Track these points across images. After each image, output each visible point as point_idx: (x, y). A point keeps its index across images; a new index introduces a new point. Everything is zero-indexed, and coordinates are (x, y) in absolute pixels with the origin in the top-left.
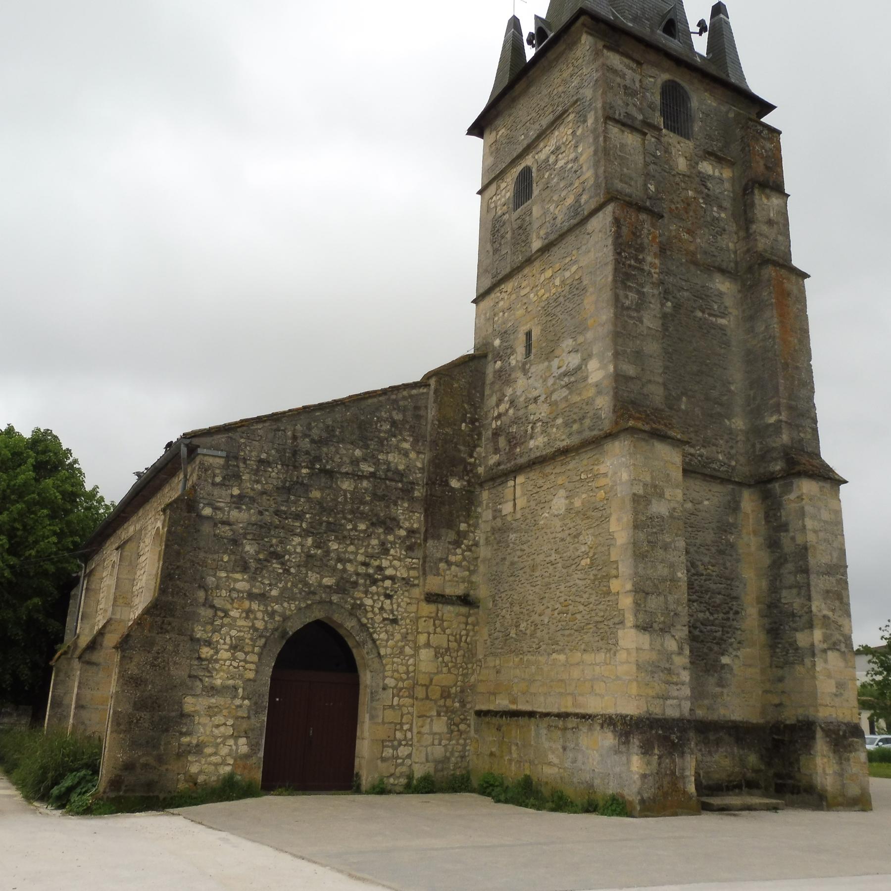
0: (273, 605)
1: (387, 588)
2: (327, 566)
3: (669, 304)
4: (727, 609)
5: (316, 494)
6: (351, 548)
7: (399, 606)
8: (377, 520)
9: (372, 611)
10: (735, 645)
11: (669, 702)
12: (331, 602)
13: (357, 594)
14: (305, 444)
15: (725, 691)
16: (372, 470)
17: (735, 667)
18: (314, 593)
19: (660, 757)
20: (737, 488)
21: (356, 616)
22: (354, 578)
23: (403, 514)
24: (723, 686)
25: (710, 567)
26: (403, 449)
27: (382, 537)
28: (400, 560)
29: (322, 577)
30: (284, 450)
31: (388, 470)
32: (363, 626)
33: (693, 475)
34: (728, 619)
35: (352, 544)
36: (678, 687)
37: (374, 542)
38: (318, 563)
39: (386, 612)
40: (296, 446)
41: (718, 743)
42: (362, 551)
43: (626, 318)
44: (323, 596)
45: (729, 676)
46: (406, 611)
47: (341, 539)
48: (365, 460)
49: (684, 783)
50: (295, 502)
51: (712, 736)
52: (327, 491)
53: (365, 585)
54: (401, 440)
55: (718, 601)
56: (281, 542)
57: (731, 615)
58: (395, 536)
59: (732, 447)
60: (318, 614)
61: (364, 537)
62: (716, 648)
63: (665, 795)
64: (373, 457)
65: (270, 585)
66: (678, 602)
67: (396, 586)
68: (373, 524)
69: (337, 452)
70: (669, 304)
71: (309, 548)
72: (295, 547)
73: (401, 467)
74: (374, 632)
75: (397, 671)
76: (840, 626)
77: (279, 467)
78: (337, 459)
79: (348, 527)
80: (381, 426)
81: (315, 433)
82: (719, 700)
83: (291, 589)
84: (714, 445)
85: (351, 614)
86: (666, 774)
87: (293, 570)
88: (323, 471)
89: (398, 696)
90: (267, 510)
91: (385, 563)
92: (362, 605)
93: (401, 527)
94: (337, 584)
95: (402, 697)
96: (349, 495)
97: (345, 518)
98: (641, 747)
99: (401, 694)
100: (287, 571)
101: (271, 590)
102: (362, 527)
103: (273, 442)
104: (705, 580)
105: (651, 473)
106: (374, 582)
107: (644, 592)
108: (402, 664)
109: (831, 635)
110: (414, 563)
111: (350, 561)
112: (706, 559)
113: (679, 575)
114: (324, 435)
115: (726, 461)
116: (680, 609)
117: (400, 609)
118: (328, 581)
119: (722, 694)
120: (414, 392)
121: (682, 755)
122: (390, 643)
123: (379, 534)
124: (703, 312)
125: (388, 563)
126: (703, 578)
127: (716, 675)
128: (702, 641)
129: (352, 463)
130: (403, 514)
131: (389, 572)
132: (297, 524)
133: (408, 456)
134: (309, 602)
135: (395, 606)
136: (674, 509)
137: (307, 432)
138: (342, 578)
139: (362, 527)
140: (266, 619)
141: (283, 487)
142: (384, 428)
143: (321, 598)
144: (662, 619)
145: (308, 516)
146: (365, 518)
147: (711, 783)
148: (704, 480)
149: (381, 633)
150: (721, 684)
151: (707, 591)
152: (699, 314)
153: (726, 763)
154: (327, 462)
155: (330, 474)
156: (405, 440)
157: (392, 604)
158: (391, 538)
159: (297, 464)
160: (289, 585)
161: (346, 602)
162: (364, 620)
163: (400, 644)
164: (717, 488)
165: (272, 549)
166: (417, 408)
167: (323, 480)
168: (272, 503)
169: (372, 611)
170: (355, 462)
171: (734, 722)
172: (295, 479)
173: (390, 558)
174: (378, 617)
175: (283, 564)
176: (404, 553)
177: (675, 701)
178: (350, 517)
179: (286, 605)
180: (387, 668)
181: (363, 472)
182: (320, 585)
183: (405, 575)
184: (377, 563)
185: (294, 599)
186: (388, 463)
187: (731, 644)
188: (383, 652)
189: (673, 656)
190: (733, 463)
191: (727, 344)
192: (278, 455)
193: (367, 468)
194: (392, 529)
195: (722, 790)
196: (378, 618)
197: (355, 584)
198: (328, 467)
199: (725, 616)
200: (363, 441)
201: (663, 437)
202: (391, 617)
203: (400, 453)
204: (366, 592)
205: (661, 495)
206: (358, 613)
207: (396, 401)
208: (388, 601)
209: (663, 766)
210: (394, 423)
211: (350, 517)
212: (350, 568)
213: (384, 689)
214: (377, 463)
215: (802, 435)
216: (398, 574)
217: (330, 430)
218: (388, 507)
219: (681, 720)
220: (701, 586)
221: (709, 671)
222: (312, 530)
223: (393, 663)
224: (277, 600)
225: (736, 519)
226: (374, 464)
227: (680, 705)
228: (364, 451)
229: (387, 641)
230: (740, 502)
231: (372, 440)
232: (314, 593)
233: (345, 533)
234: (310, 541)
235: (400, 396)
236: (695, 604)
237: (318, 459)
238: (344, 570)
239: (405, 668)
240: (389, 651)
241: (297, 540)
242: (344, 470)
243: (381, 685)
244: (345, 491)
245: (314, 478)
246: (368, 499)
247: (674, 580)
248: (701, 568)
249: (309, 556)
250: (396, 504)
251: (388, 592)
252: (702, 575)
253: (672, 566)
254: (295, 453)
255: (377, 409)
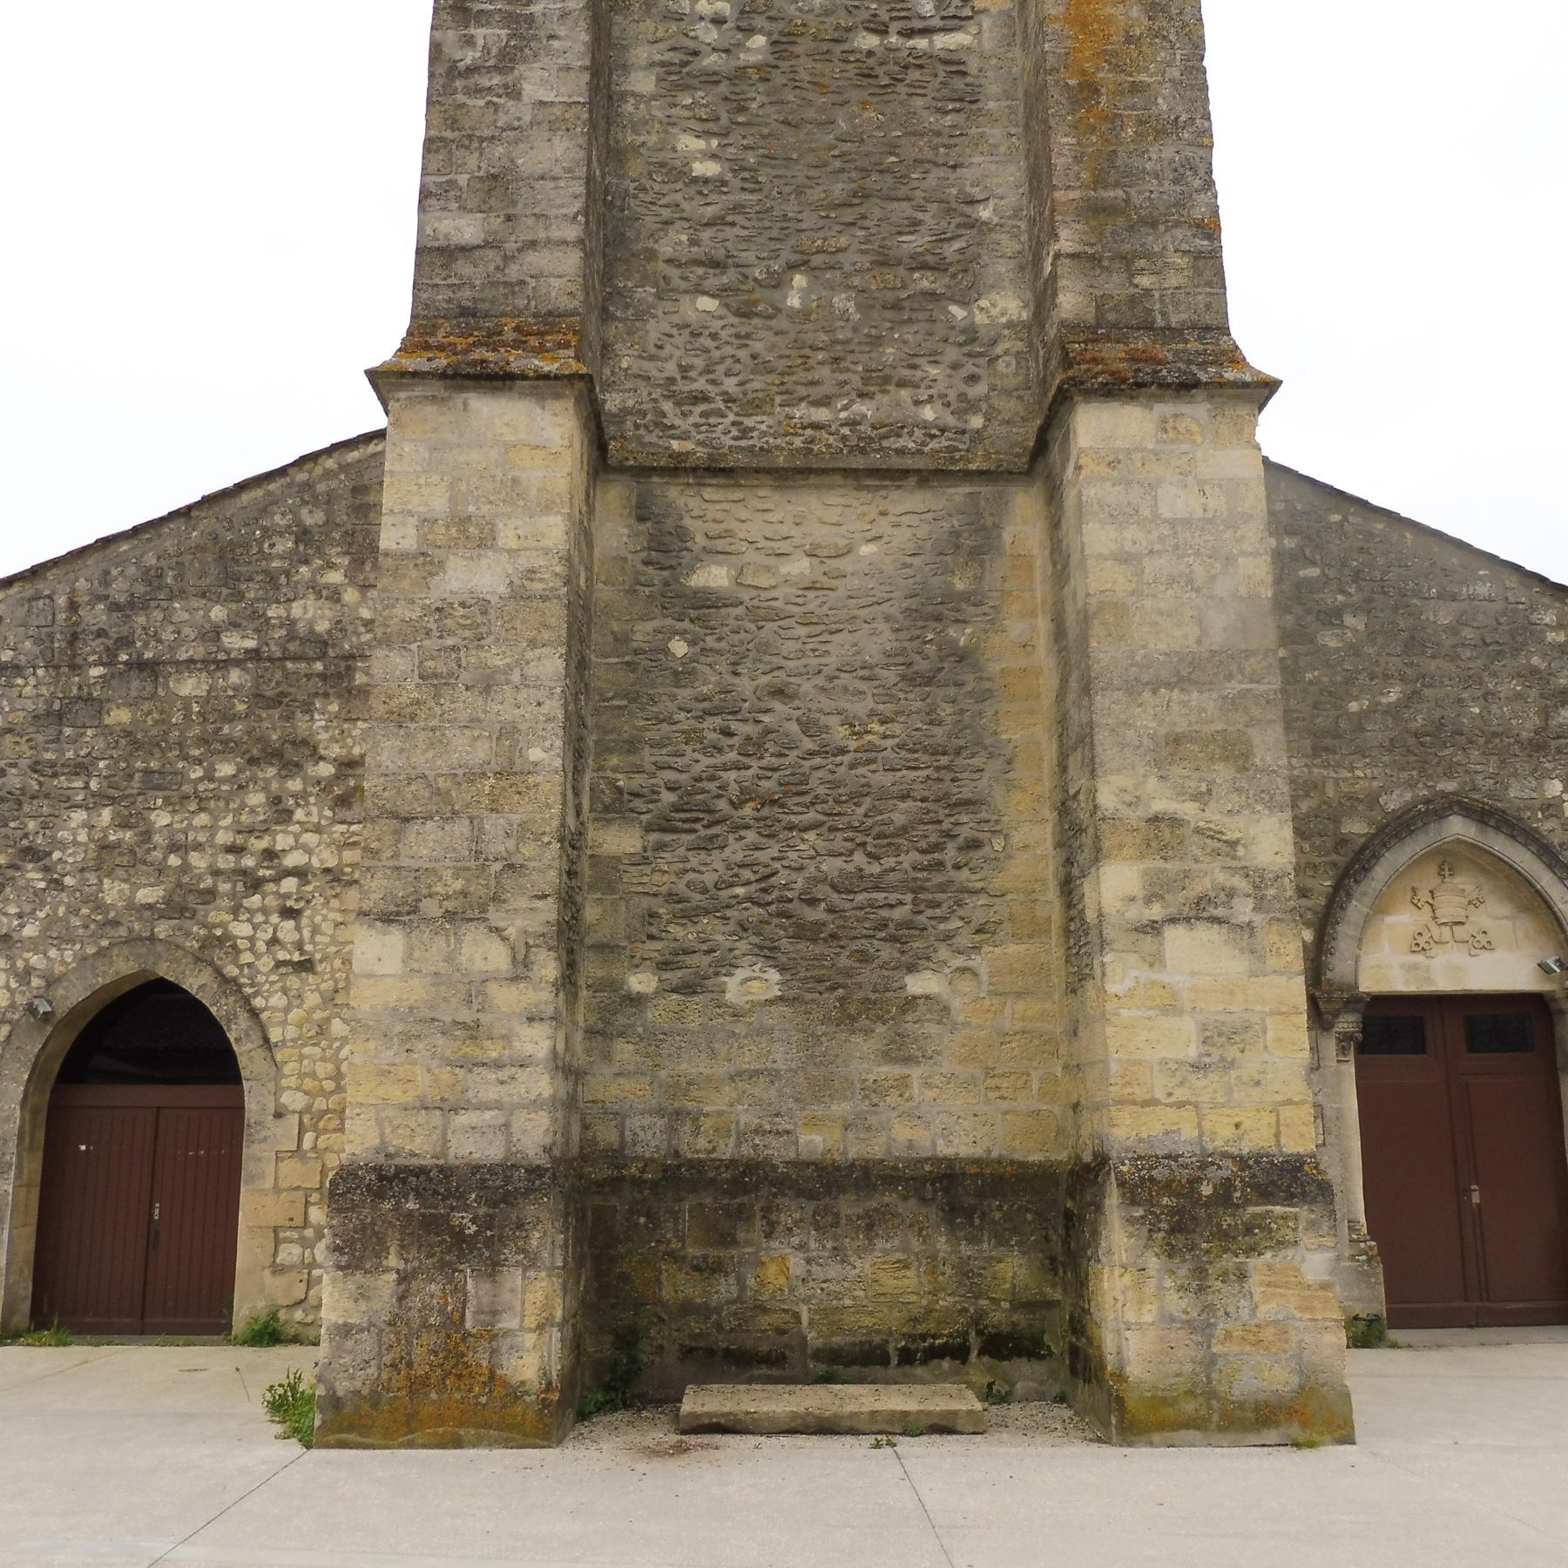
0: (27, 955)
1: (287, 896)
2: (145, 862)
3: (759, 41)
4: (933, 839)
5: (120, 716)
6: (202, 819)
7: (315, 930)
8: (263, 750)
9: (252, 949)
10: (964, 940)
11: (463, 1119)
12: (152, 938)
13: (214, 917)
14: (97, 616)
15: (916, 1073)
16: (251, 644)
17: (956, 1003)
18: (115, 923)
19: (404, 1278)
20: (985, 490)
21: (212, 964)
22: (208, 882)
23: (326, 728)
24: (908, 1060)
25: (876, 727)
26: (327, 586)
27: (274, 786)
28: (318, 829)
29: (135, 888)
30: (51, 636)
31: (292, 636)
32: (224, 980)
33: (813, 480)
34: (939, 865)
35: (201, 809)
36: (503, 1074)
37: (256, 799)
38: (125, 860)
39: (283, 947)
40: (77, 624)
41: (871, 1225)
42: (227, 821)
43: (461, 98)
44: (137, 926)
45: (932, 1029)
46: (334, 941)
47: (176, 803)
48: (234, 625)
49: (494, 1352)
50: (73, 741)
51: (848, 1206)
52: (146, 706)
53: (233, 895)
54: (322, 568)
55: (899, 819)
56: (44, 826)
57: (950, 854)
58: (305, 780)
59: (973, 379)
60: (124, 966)
61: (230, 792)
62: (887, 952)
63: (416, 1386)
64: (254, 615)
65: (20, 916)
66: (523, 831)
67: (309, 888)
68: (252, 761)
69: (167, 619)
70: (759, 41)
71: (105, 830)
72: (74, 832)
73: (322, 627)
74: (256, 994)
75: (313, 1075)
76: (1233, 844)
77: (40, 672)
78: (168, 635)
79: (193, 776)
80: (272, 546)
81: (119, 590)
82: (892, 1099)
83: (65, 919)
84: (902, 384)
85: (198, 960)
86: (425, 1326)
87: (68, 881)
88: (141, 666)
89: (315, 1128)
90: (14, 765)
91: (282, 841)
92: (227, 936)
93: (322, 758)
94: (168, 901)
95: (326, 1130)
96: (196, 708)
97: (186, 758)
98: (337, 1249)
99: (321, 1124)
100: (57, 884)
101: (22, 926)
102: (226, 769)
103: (25, 625)
104: (852, 766)
105: (452, 486)
106: (256, 885)
107: (394, 815)
108: (323, 1059)
109: (1186, 874)
110: (354, 834)
111: (198, 847)
112: (861, 708)
113: (535, 754)
114: (140, 589)
115: (951, 421)
116: (528, 849)
117: (318, 938)
118: (146, 895)
119: (904, 1082)
120: (353, 456)
121: (493, 1268)
122: (295, 1014)
123: (267, 781)
124: (883, 32)
125: (291, 840)
126: (847, 759)
127: (880, 1029)
128: (833, 936)
129: (202, 636)
130: (326, 728)
131: (293, 860)
132: (79, 784)
133: (338, 601)
134: (105, 943)
135: (306, 933)
136: (530, 574)
137: (101, 591)
138: (179, 885)
139: (226, 769)
140: (13, 985)
141: (48, 714)
142: (279, 548)
143: (131, 930)
144: (458, 885)
145: (102, 764)
146: (232, 751)
147: (837, 1340)
148: (859, 488)
149: (271, 994)
150: (900, 1052)
151: (856, 797)
152: (870, 41)
153: (909, 1284)
154: (146, 644)
155: (150, 669)
156: (331, 566)
157: (298, 928)
158: (295, 785)
159: (78, 660)
160: (61, 911)
161: (187, 934)
162: (231, 970)
163: (318, 1015)
164: (909, 501)
165: (25, 842)
166: (356, 491)
167: (135, 684)
168: (25, 747)
169: (252, 949)
170: (213, 634)
171: (950, 1162)
172: (75, 691)
173: (295, 828)
174: (264, 959)
175: (46, 869)
176: (328, 813)
177: (488, 1115)
178: (197, 752)
179: (53, 953)
180: (286, 1070)
181: (228, 652)
182: (131, 906)
183: (332, 863)
184: (264, 843)
185: (72, 941)
186: (290, 623)
187: (947, 937)
188: (275, 1035)
189: (492, 988)
190: (977, 422)
191: (968, 100)
192: (37, 650)
193: (236, 642)
194: (297, 765)
195: (884, 1361)
196: (265, 963)
197: (211, 893)
198: (148, 655)
199: (925, 860)
200: (229, 583)
201: (497, 380)
202: (296, 957)
203: (319, 596)
204: (235, 911)
205: (486, 542)
206: (217, 954)
207: (308, 485)
208: (290, 924)
209: (415, 1302)
210: (303, 535)
211: (197, 752)
212: (198, 861)
213: (278, 1115)
214: (263, 625)
215: (1145, 281)
216: (315, 862)
217: (153, 578)
218: (289, 718)
219: (505, 1169)
220: (836, 785)
221: (853, 1019)
222: (112, 792)
223: (302, 1057)
224: (35, 945)
225: (979, 579)
226: (256, 630)
227: (507, 1125)
228: (234, 606)
229: (287, 1010)
230: (997, 527)
231: (250, 579)
232: (115, 923)
233: (187, 788)
234: (106, 814)
235: (319, 470)
236: (811, 836)
237: (126, 642)
238: (185, 868)
239: (330, 1066)
240: (291, 1032)
241: (79, 816)
242: (183, 655)
243: (271, 1108)
244: (187, 701)
245: (114, 683)
246: (241, 707)
247: (511, 773)
248: (840, 734)
249: (105, 847)
250: (308, 709)
251: (289, 903)
252: (843, 751)
253: (508, 732)
254: (73, 638)
255: (264, 511)
